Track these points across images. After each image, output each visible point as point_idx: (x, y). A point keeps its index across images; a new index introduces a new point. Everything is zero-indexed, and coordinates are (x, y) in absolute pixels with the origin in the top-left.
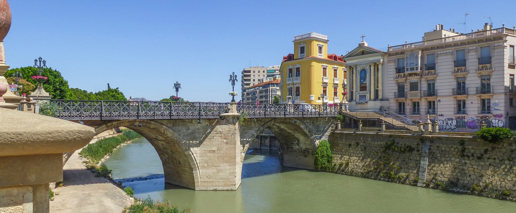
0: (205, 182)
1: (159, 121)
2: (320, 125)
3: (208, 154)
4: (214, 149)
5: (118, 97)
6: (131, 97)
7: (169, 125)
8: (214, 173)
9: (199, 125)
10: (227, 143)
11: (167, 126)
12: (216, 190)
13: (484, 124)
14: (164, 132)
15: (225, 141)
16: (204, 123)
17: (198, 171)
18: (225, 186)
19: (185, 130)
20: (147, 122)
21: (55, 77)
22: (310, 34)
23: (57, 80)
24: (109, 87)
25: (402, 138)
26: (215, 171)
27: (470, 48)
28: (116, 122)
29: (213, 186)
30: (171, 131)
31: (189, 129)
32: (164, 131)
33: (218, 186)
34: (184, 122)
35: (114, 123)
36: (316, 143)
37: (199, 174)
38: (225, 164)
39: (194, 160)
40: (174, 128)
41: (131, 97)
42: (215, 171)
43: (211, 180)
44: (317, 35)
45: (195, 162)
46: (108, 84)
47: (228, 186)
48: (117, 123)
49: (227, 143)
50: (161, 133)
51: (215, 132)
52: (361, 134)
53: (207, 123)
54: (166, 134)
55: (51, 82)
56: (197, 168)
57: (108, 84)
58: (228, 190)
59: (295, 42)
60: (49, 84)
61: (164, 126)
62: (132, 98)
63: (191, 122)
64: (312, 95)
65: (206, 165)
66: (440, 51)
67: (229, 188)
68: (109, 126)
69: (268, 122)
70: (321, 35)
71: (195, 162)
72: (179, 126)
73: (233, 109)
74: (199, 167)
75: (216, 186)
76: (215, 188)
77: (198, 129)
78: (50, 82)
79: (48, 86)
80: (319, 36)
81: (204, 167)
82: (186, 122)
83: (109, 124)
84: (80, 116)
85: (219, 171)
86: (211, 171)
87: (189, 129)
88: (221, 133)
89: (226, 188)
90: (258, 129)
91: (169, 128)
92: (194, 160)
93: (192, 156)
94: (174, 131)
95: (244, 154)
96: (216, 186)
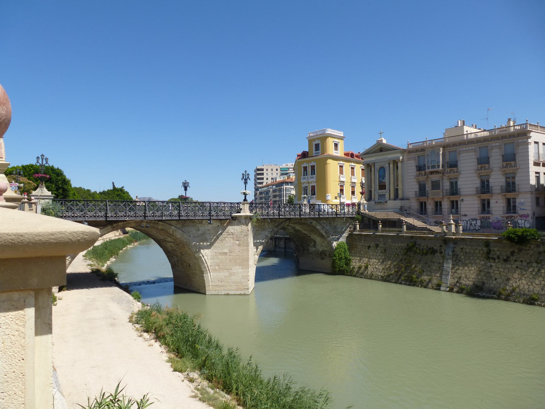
0: (217, 286)
1: (168, 222)
3: (220, 257)
4: (226, 251)
6: (137, 197)
7: (178, 226)
8: (225, 277)
9: (210, 225)
10: (239, 245)
11: (176, 227)
15: (237, 242)
16: (215, 224)
17: (209, 274)
18: (237, 290)
19: (195, 231)
20: (154, 223)
21: (58, 176)
26: (227, 274)
28: (122, 223)
29: (225, 290)
31: (199, 230)
32: (173, 232)
33: (230, 290)
35: (120, 224)
36: (334, 245)
37: (210, 277)
38: (238, 267)
39: (205, 263)
41: (137, 197)
42: (227, 274)
43: (222, 284)
46: (113, 183)
48: (123, 224)
49: (239, 245)
51: (227, 234)
54: (174, 235)
56: (208, 271)
57: (113, 183)
58: (241, 295)
61: (172, 227)
62: (138, 197)
64: (328, 195)
65: (217, 268)
66: (472, 146)
67: (242, 292)
70: (337, 131)
74: (210, 270)
75: (228, 290)
76: (227, 292)
77: (209, 230)
78: (52, 180)
80: (334, 132)
82: (196, 222)
83: (115, 225)
84: (84, 217)
86: (223, 274)
87: (199, 230)
88: (232, 234)
89: (238, 292)
90: (271, 230)
91: (178, 228)
92: (205, 263)
93: (203, 259)
94: (183, 232)
96: (228, 290)
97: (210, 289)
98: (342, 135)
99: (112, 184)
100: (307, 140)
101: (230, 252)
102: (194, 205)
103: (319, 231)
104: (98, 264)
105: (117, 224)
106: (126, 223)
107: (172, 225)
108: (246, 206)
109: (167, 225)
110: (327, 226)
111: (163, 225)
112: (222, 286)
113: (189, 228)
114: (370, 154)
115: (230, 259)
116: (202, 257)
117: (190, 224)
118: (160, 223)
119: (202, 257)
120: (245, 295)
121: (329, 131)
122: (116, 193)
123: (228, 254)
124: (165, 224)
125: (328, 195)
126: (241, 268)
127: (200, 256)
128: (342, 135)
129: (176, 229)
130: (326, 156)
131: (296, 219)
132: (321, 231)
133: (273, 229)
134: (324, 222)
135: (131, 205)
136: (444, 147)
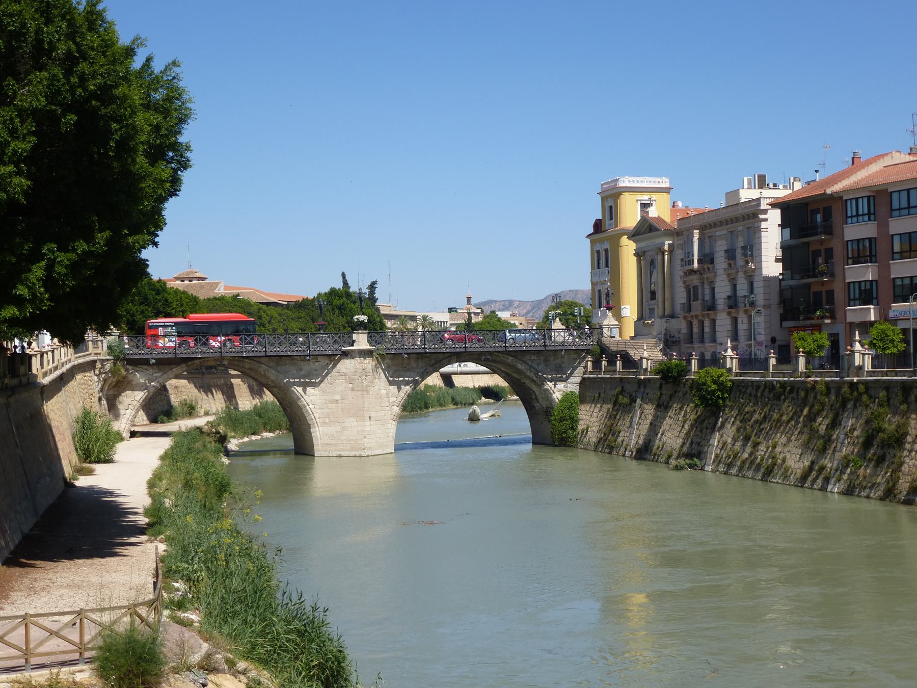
0: (327, 444)
1: (255, 359)
2: (563, 366)
3: (330, 406)
4: (337, 397)
5: (352, 309)
6: (469, 300)
7: (271, 365)
8: (337, 432)
9: (317, 364)
10: (353, 389)
11: (267, 366)
12: (340, 456)
13: (675, 357)
14: (265, 374)
15: (351, 386)
16: (323, 361)
17: (317, 428)
18: (352, 449)
19: (295, 371)
20: (239, 361)
21: (158, 293)
22: (617, 180)
23: (159, 297)
24: (345, 283)
25: (629, 383)
26: (338, 428)
27: (718, 234)
28: (198, 361)
29: (336, 450)
30: (274, 372)
31: (301, 370)
32: (264, 371)
33: (343, 450)
34: (293, 359)
35: (196, 361)
36: (555, 397)
37: (318, 433)
38: (352, 419)
39: (311, 413)
40: (279, 368)
41: (469, 300)
42: (338, 428)
43: (334, 442)
44: (634, 181)
45: (313, 417)
46: (343, 275)
47: (356, 450)
48: (200, 362)
49: (353, 389)
50: (261, 374)
51: (338, 374)
52: (603, 377)
53: (327, 362)
54: (267, 375)
55: (151, 301)
56: (316, 425)
57: (343, 275)
58: (355, 456)
59: (603, 195)
60: (148, 305)
61: (263, 365)
62: (473, 301)
63: (304, 360)
64: (624, 307)
65: (327, 421)
66: (720, 231)
67: (357, 454)
68: (190, 365)
69: (444, 359)
70: (646, 179)
71: (313, 417)
72: (285, 365)
73: (361, 340)
74: (319, 423)
75: (340, 450)
76: (338, 453)
77: (316, 370)
78: (149, 301)
79: (147, 307)
80: (641, 182)
81: (324, 423)
82: (296, 360)
83: (190, 363)
84: (151, 354)
85: (344, 429)
86: (334, 429)
87: (301, 370)
88: (345, 375)
89: (353, 454)
90: (422, 370)
91: (270, 367)
92: (311, 413)
93: (308, 407)
94: (278, 371)
95: (398, 408)
96: (340, 450)
97: (319, 450)
98: (667, 185)
99: (341, 278)
100: (599, 198)
101: (342, 399)
102: (411, 333)
103: (524, 373)
104: (126, 371)
105: (193, 362)
106: (204, 361)
107: (262, 363)
108: (361, 337)
109: (256, 363)
110: (539, 364)
111: (251, 363)
112: (334, 445)
113: (287, 366)
114: (642, 234)
115: (342, 409)
116: (306, 405)
117: (287, 362)
118: (246, 360)
119: (306, 405)
120: (360, 456)
121: (625, 182)
122: (336, 302)
123: (339, 401)
124: (252, 362)
125: (624, 307)
126: (355, 420)
127: (304, 405)
128: (665, 185)
129: (268, 368)
130: (620, 232)
131: (472, 354)
132: (528, 373)
133: (426, 369)
134: (533, 358)
135: (249, 339)
136: (702, 229)
